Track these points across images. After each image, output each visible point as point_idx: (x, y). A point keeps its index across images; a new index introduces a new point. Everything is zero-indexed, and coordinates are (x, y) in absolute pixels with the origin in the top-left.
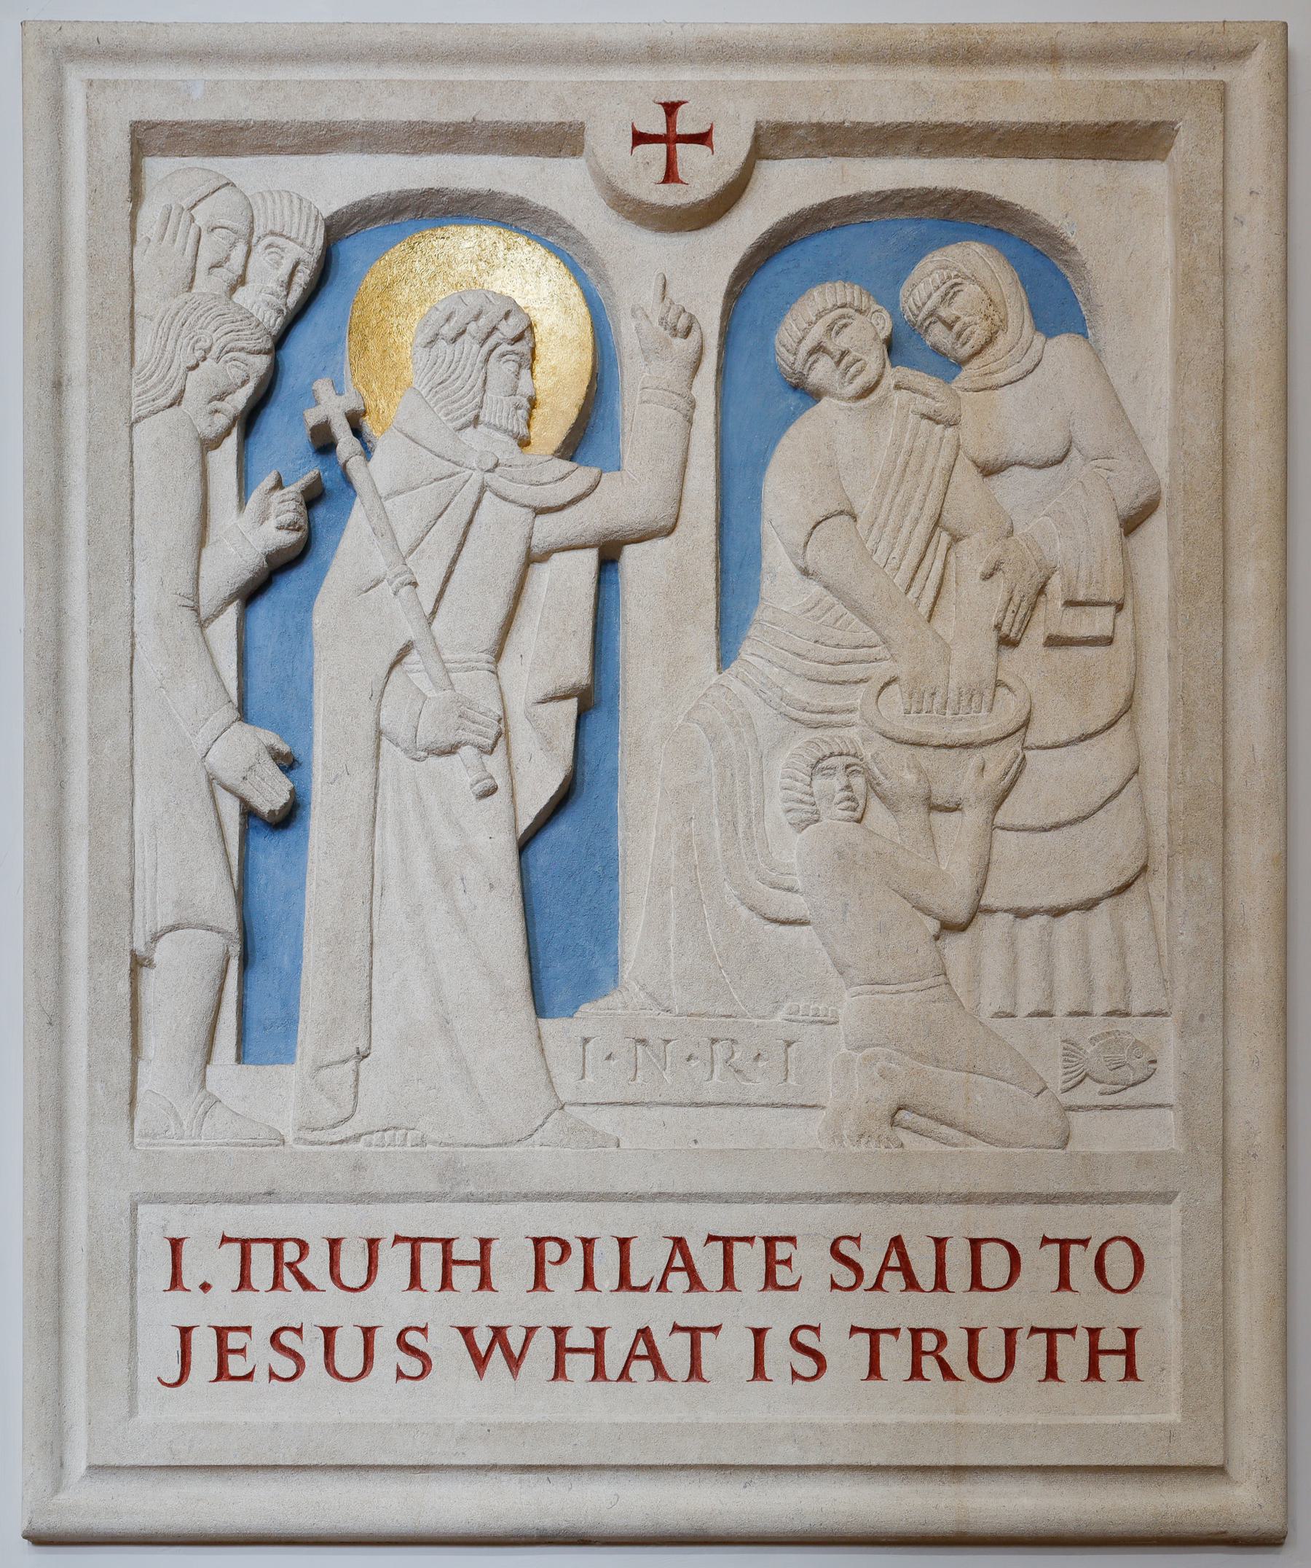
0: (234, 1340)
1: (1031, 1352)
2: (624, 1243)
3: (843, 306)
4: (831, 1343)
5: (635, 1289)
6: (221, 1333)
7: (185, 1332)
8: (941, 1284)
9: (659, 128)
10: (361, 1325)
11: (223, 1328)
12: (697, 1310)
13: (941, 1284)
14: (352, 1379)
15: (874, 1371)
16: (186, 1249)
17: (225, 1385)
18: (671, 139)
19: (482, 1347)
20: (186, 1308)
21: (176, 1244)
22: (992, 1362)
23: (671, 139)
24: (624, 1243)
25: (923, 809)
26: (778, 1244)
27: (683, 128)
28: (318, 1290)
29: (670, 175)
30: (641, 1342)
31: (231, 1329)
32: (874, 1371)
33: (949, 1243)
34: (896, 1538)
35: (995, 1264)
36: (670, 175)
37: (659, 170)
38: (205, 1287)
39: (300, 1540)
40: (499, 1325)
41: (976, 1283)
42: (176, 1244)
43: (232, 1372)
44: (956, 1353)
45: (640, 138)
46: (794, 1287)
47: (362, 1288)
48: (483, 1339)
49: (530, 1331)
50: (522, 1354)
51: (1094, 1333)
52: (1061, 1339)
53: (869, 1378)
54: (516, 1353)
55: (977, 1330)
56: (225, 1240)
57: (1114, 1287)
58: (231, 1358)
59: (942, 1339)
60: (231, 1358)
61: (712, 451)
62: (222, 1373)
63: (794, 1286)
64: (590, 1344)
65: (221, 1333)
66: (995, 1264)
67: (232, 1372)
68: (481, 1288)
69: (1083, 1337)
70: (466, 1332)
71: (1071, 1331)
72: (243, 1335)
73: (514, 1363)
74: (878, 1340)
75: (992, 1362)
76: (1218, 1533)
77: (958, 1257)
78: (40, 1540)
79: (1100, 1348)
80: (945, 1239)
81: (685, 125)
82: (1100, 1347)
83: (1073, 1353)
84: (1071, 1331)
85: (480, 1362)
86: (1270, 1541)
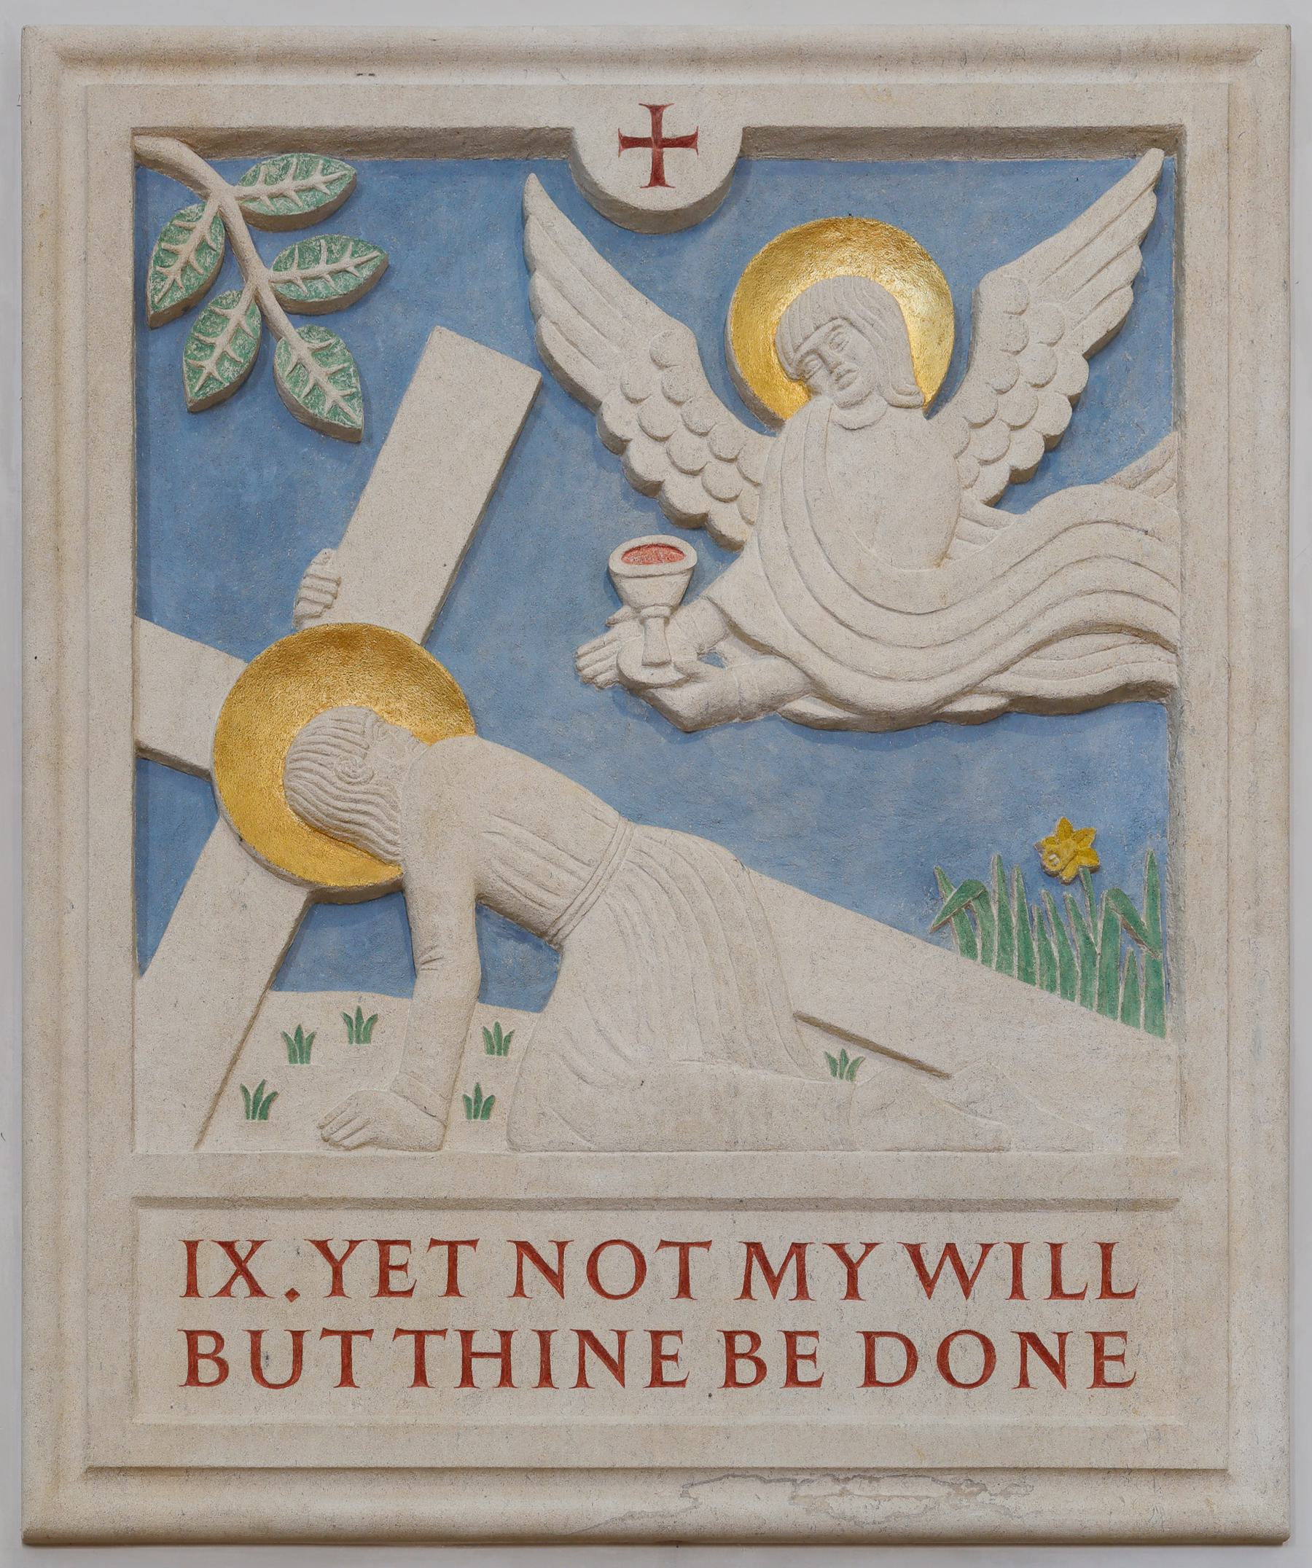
1: (322, 1354)
3: (833, 319)
6: (657, 1336)
9: (646, 132)
10: (616, 1329)
11: (731, 1332)
15: (420, 1377)
16: (1064, 1253)
17: (794, 1390)
18: (659, 142)
19: (931, 1270)
20: (865, 1315)
21: (1056, 1248)
22: (277, 1369)
23: (659, 142)
25: (225, 789)
26: (691, 1249)
28: (413, 1288)
29: (657, 178)
32: (420, 1377)
33: (1064, 1248)
36: (657, 178)
38: (292, 1294)
42: (1056, 1248)
43: (801, 1378)
44: (237, 1353)
49: (986, 1248)
51: (467, 1336)
52: (430, 1342)
53: (540, 1385)
54: (776, 1272)
55: (549, 1333)
57: (608, 1291)
59: (755, 1339)
60: (665, 1364)
61: (511, 438)
62: (1099, 1380)
63: (1081, 1293)
64: (497, 1348)
65: (1098, 1338)
67: (666, 1378)
68: (188, 1294)
69: (455, 1341)
71: (443, 1333)
72: (1119, 1340)
73: (967, 1284)
74: (350, 1340)
75: (277, 1369)
79: (1105, 1354)
80: (1060, 1245)
83: (444, 1354)
84: (443, 1333)
85: (928, 1283)
86: (1274, 1541)
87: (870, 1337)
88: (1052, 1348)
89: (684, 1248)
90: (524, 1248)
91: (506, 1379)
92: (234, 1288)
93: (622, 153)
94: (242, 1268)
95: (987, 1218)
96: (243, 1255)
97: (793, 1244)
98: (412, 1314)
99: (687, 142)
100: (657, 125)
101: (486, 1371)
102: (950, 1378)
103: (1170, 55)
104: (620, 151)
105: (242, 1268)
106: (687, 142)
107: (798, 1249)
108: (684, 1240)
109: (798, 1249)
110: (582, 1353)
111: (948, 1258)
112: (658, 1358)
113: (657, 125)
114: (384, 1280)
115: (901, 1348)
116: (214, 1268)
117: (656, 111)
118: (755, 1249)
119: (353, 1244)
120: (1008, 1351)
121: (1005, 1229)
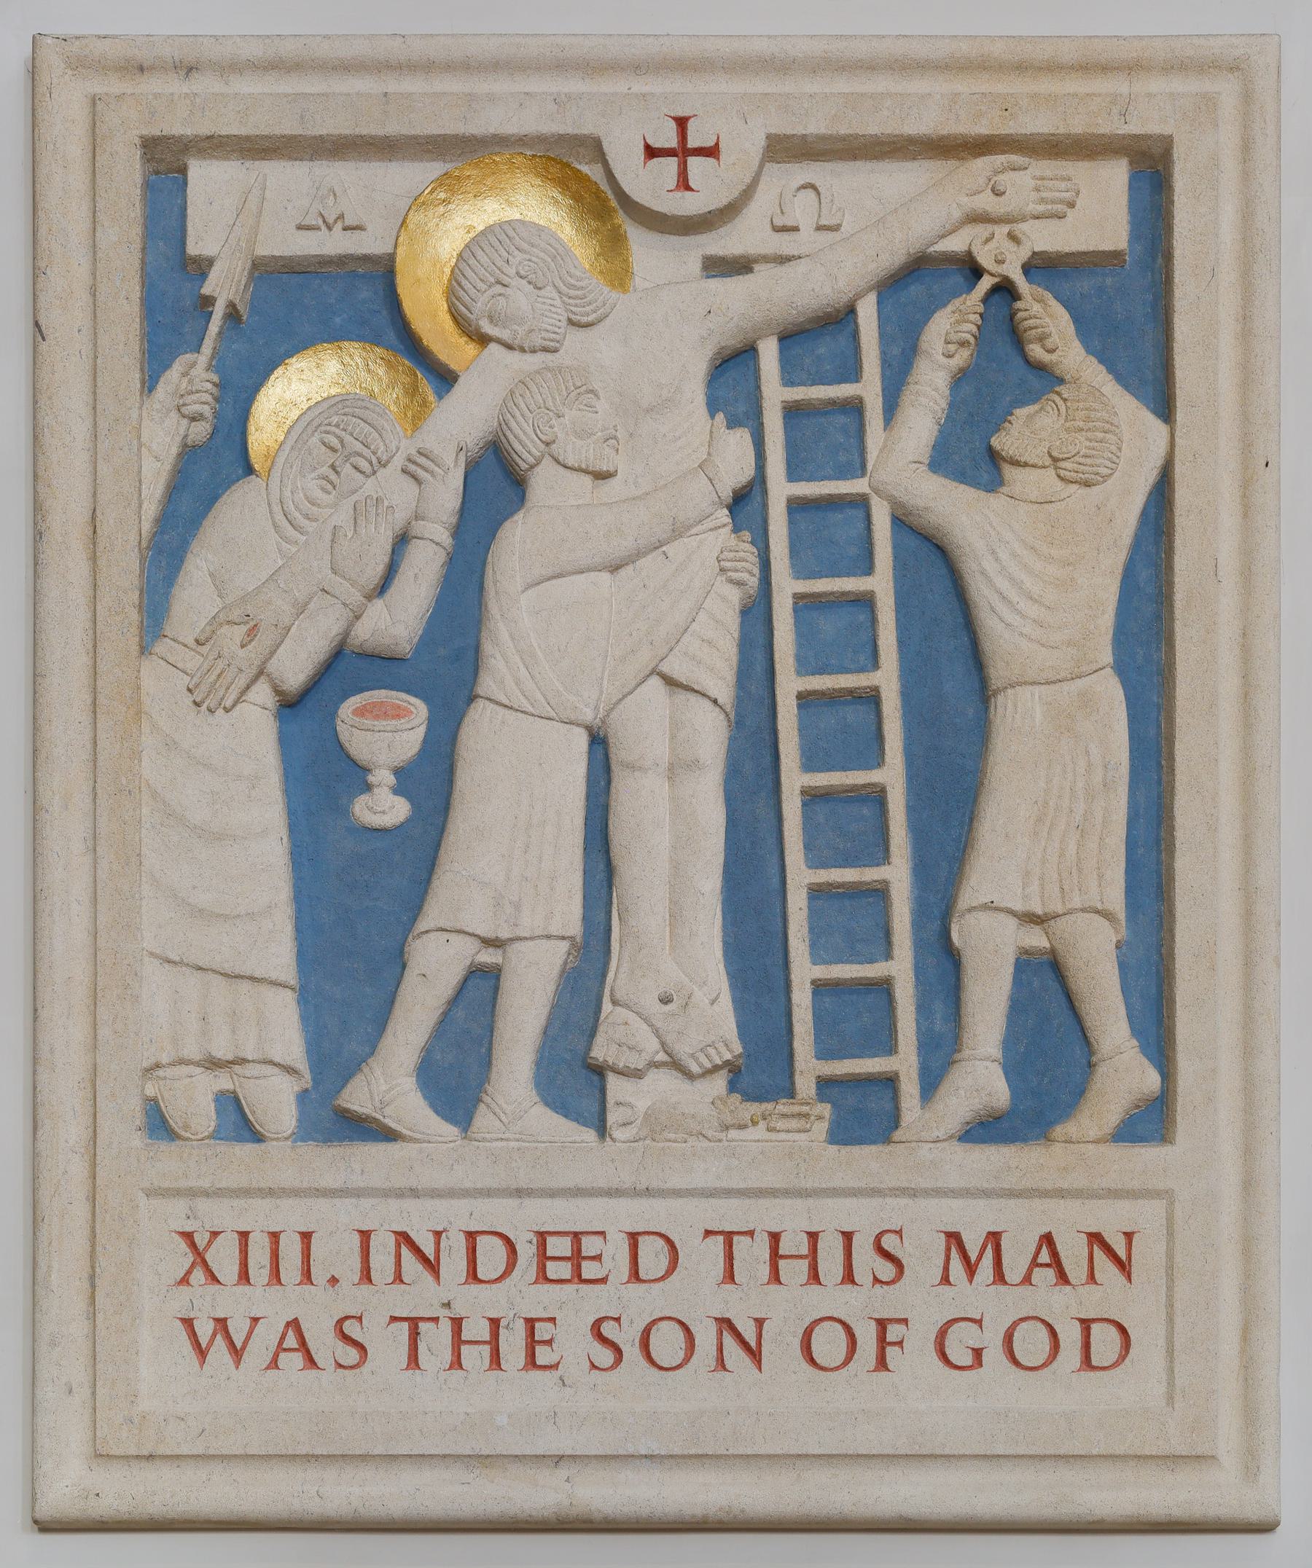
0: (542, 1331)
2: (306, 1237)
4: (373, 1333)
5: (644, 1281)
6: (530, 1323)
7: (365, 1236)
8: (244, 1277)
12: (539, 1300)
13: (244, 1277)
14: (1107, 1367)
17: (535, 1375)
18: (683, 152)
19: (204, 1343)
24: (306, 1237)
27: (692, 143)
29: (684, 183)
30: (290, 1333)
31: (1094, 1320)
34: (484, 1522)
35: (653, 1257)
37: (672, 181)
39: (960, 1527)
40: (496, 1317)
41: (1087, 1362)
45: (651, 152)
46: (603, 1281)
47: (662, 1278)
48: (205, 1329)
50: (244, 1347)
56: (708, 1233)
58: (539, 1349)
60: (549, 1265)
62: (531, 1362)
63: (603, 1279)
65: (530, 1323)
66: (653, 1257)
69: (446, 1327)
70: (188, 1323)
72: (902, 1327)
74: (417, 1327)
76: (513, 1523)
77: (617, 1251)
78: (45, 1527)
81: (668, 139)
82: (549, 1253)
83: (436, 1339)
85: (202, 1353)
86: (1265, 1528)
87: (471, 1236)
88: (750, 1335)
89: (729, 1236)
90: (1096, 1239)
91: (814, 1277)
92: (192, 1279)
93: (647, 164)
94: (200, 1259)
95: (441, 1205)
96: (201, 1247)
97: (989, 1233)
98: (595, 1302)
99: (711, 152)
100: (669, 153)
101: (475, 1357)
102: (1016, 1363)
103: (1081, 67)
104: (645, 163)
105: (200, 1259)
106: (711, 152)
107: (994, 1238)
108: (728, 1229)
109: (994, 1238)
110: (759, 1336)
111: (1095, 1247)
112: (532, 1343)
113: (669, 153)
114: (542, 1270)
115: (1113, 1332)
116: (224, 1258)
117: (682, 123)
118: (954, 1238)
119: (215, 1234)
120: (706, 1336)
121: (350, 1214)
